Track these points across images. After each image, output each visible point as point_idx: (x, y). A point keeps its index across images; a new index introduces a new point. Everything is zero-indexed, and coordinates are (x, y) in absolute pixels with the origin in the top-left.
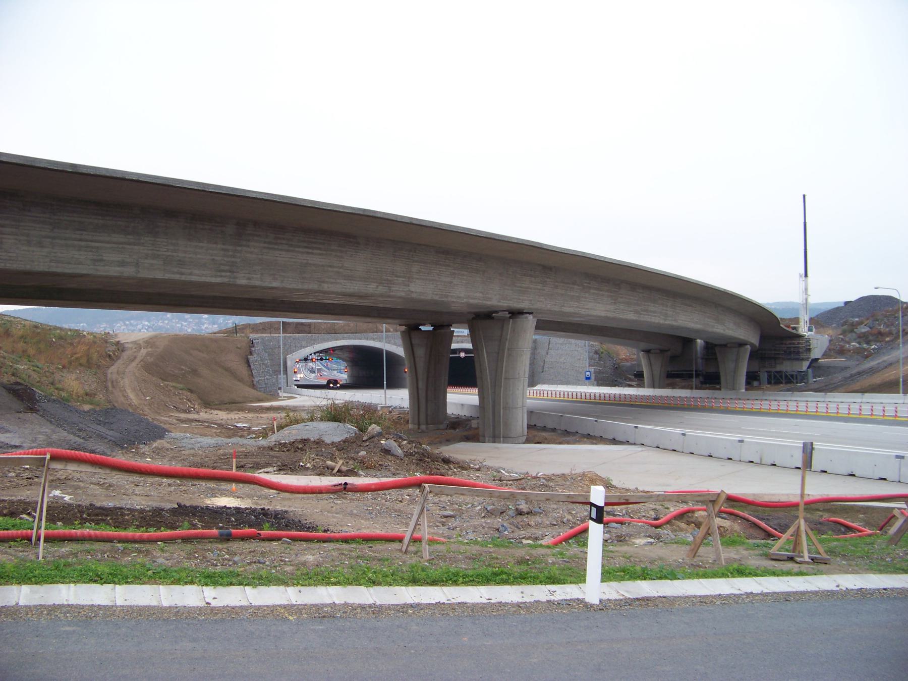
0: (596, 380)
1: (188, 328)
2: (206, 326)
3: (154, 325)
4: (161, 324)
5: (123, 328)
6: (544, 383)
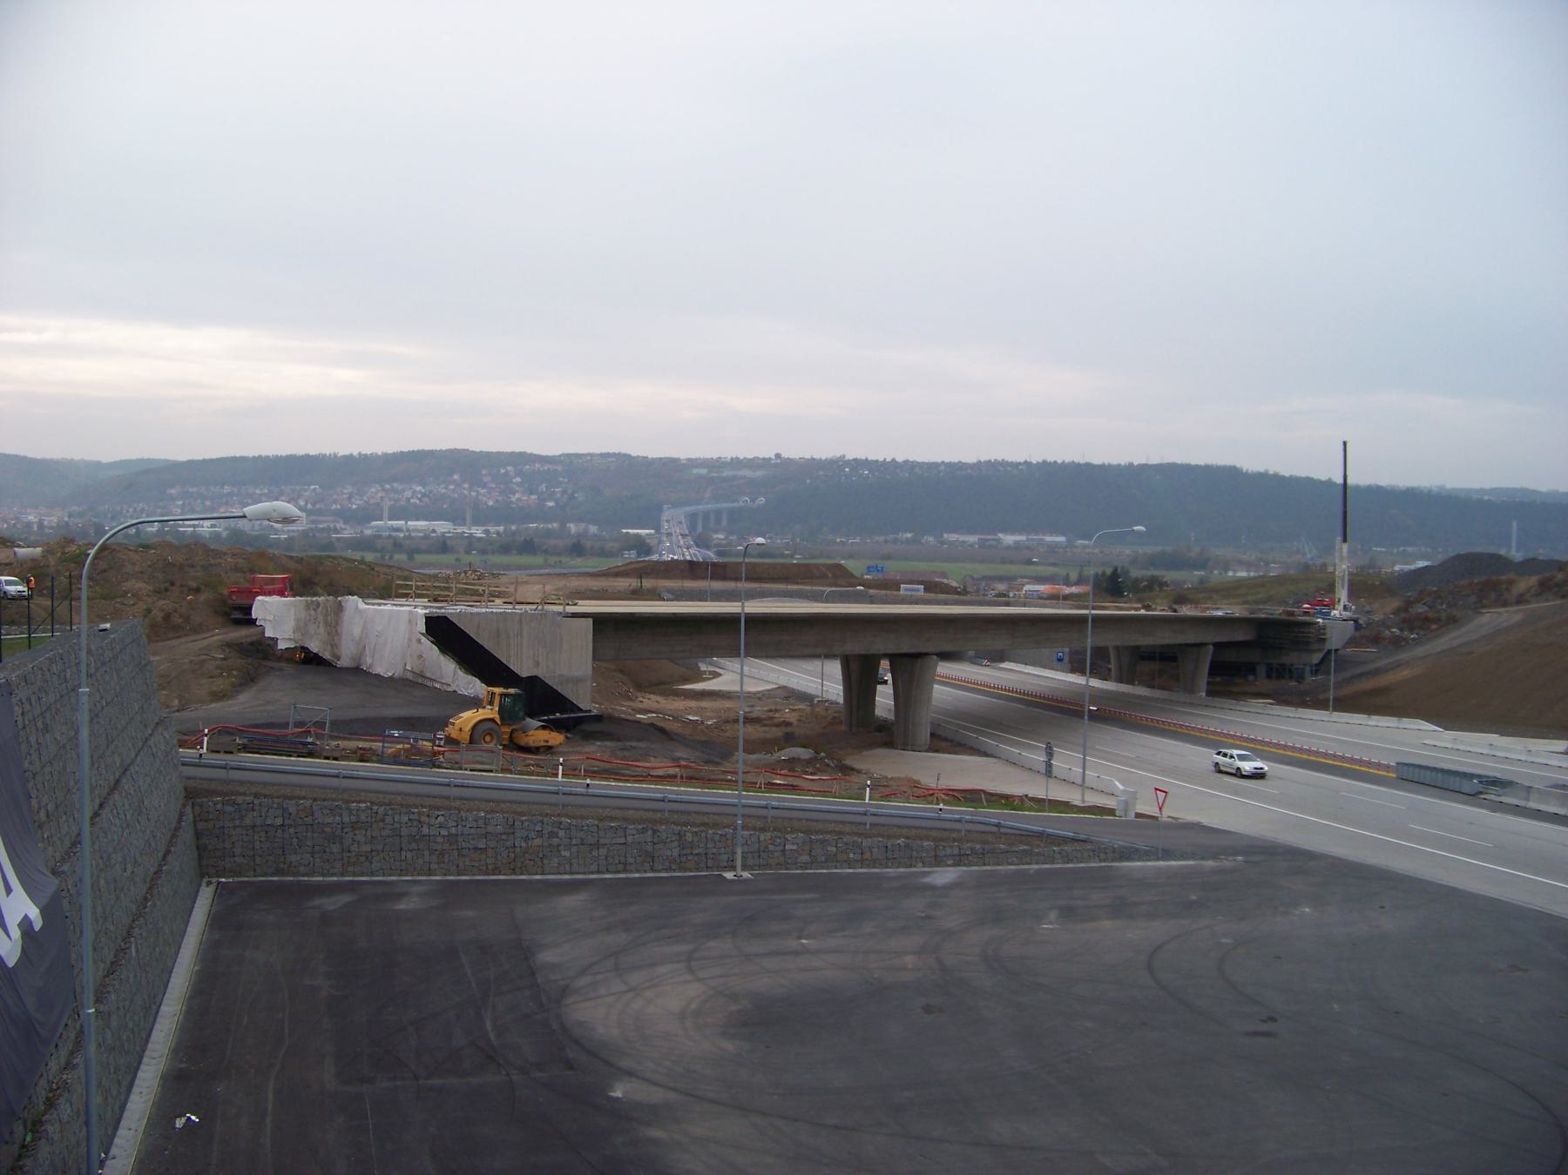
0: (1071, 662)
1: (489, 498)
2: (517, 495)
3: (431, 492)
4: (444, 491)
5: (380, 495)
6: (1010, 661)
